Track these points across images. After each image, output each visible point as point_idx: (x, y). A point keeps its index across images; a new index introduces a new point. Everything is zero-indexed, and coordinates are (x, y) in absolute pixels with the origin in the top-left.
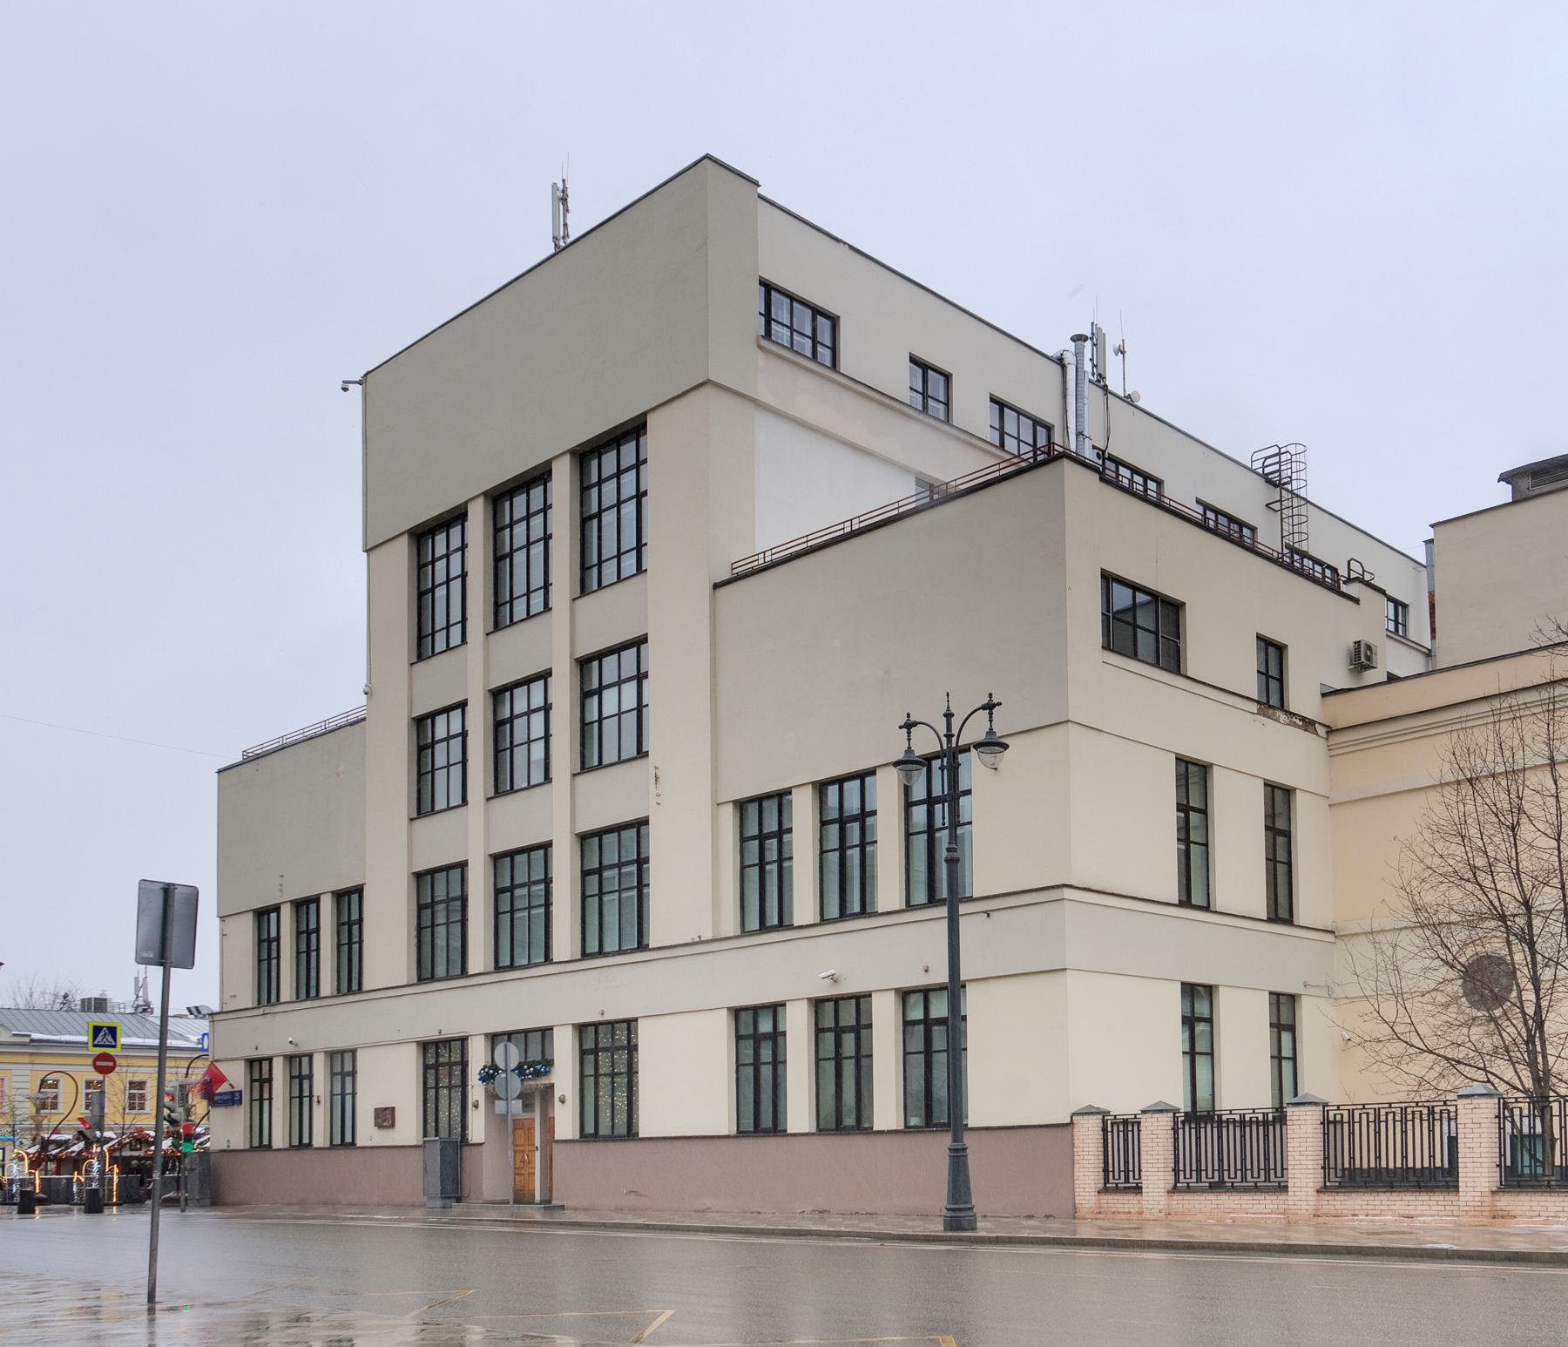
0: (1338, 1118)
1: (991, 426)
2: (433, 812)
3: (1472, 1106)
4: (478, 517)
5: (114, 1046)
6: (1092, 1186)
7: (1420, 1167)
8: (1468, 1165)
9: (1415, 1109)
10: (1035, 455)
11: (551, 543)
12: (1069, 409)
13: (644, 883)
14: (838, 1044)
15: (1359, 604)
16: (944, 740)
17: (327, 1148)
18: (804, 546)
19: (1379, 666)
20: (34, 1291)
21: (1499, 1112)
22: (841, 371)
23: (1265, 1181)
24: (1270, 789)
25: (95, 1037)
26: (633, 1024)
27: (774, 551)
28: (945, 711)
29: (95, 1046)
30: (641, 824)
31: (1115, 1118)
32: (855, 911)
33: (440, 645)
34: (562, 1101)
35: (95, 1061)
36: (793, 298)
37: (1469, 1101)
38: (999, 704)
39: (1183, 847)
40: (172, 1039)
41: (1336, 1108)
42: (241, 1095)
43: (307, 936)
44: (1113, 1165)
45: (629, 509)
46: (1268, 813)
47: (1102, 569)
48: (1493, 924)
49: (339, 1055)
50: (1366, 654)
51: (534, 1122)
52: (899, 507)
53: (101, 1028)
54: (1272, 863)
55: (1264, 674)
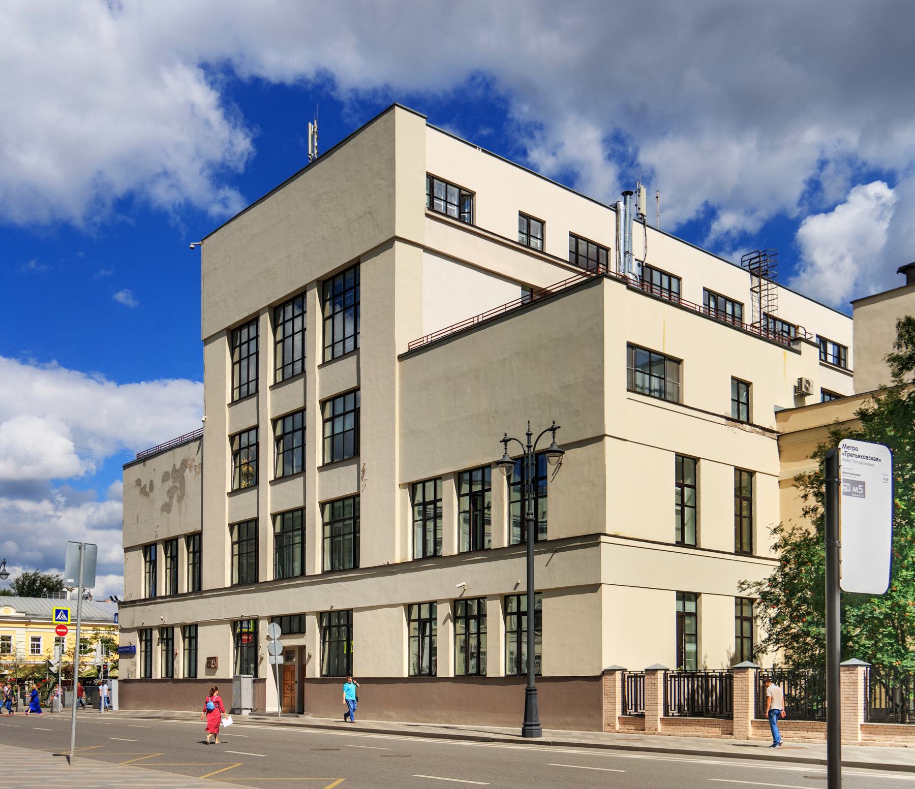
5: (67, 621)
10: (532, 296)
11: (306, 333)
14: (467, 627)
15: (800, 354)
16: (526, 449)
22: (685, 404)
25: (57, 615)
26: (486, 470)
27: (433, 335)
29: (56, 620)
31: (630, 673)
32: (408, 561)
35: (57, 628)
36: (448, 183)
38: (559, 427)
39: (679, 508)
40: (135, 674)
45: (298, 337)
49: (515, 598)
50: (805, 386)
51: (75, 744)
52: (566, 284)
53: (60, 610)
54: (448, 200)
55: (736, 401)
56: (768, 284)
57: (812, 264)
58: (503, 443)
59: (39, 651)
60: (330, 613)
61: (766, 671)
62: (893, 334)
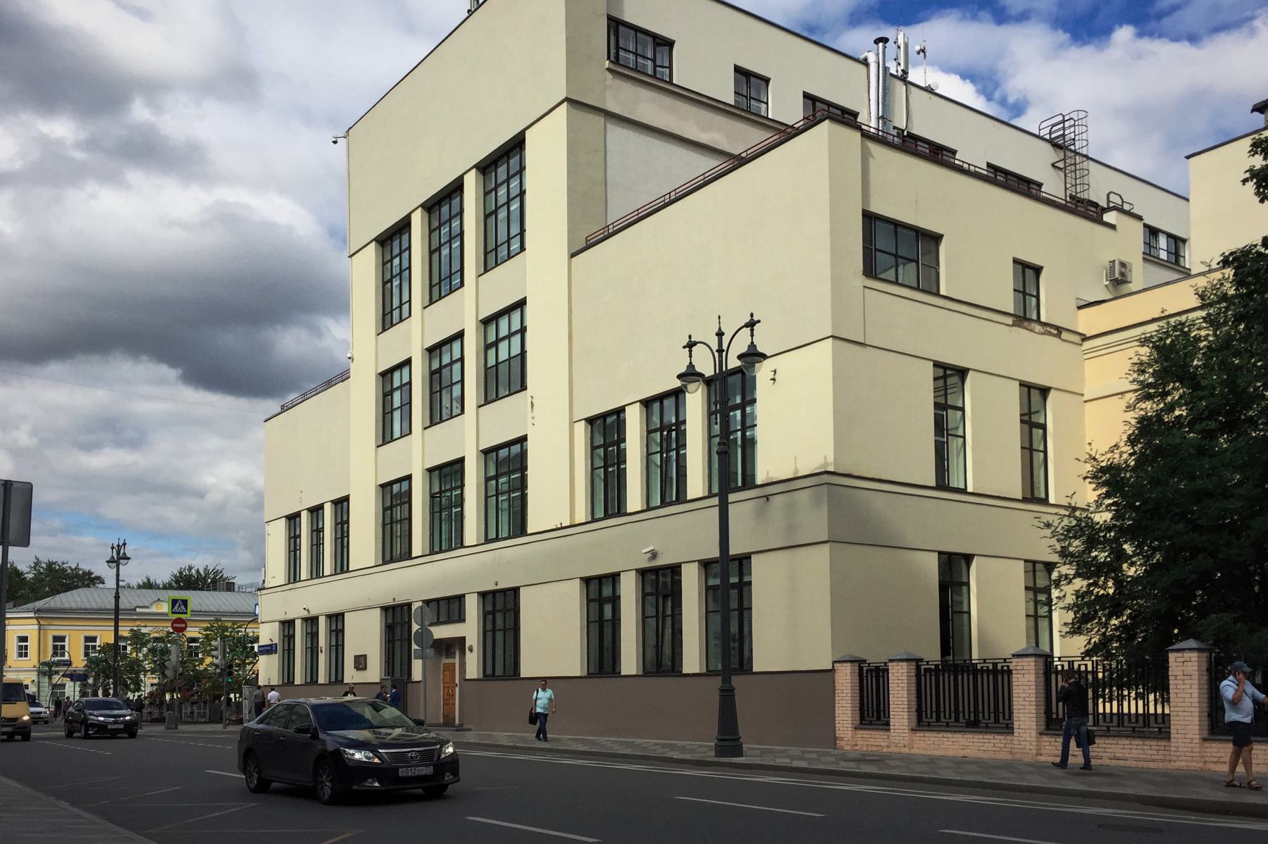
0: (1083, 668)
1: (1187, 200)
2: (392, 440)
3: (1182, 660)
4: (471, 185)
5: (186, 613)
6: (850, 722)
7: (1142, 712)
8: (1180, 713)
9: (1162, 725)
11: (528, 335)
12: (654, 651)
13: (745, 607)
15: (346, 499)
17: (327, 685)
18: (637, 217)
19: (1133, 281)
20: (731, 737)
21: (657, 612)
23: (1119, 726)
24: (1026, 389)
25: (173, 607)
28: (717, 330)
29: (173, 613)
30: (523, 440)
33: (395, 320)
34: (471, 650)
37: (1180, 655)
41: (1003, 661)
42: (276, 646)
43: (313, 636)
44: (633, 217)
46: (617, 621)
47: (735, 65)
48: (1226, 462)
51: (973, 725)
53: (177, 600)
56: (1075, 156)
57: (1071, 45)
58: (687, 349)
59: (26, 655)
60: (494, 592)
61: (1060, 660)
62: (678, 380)
